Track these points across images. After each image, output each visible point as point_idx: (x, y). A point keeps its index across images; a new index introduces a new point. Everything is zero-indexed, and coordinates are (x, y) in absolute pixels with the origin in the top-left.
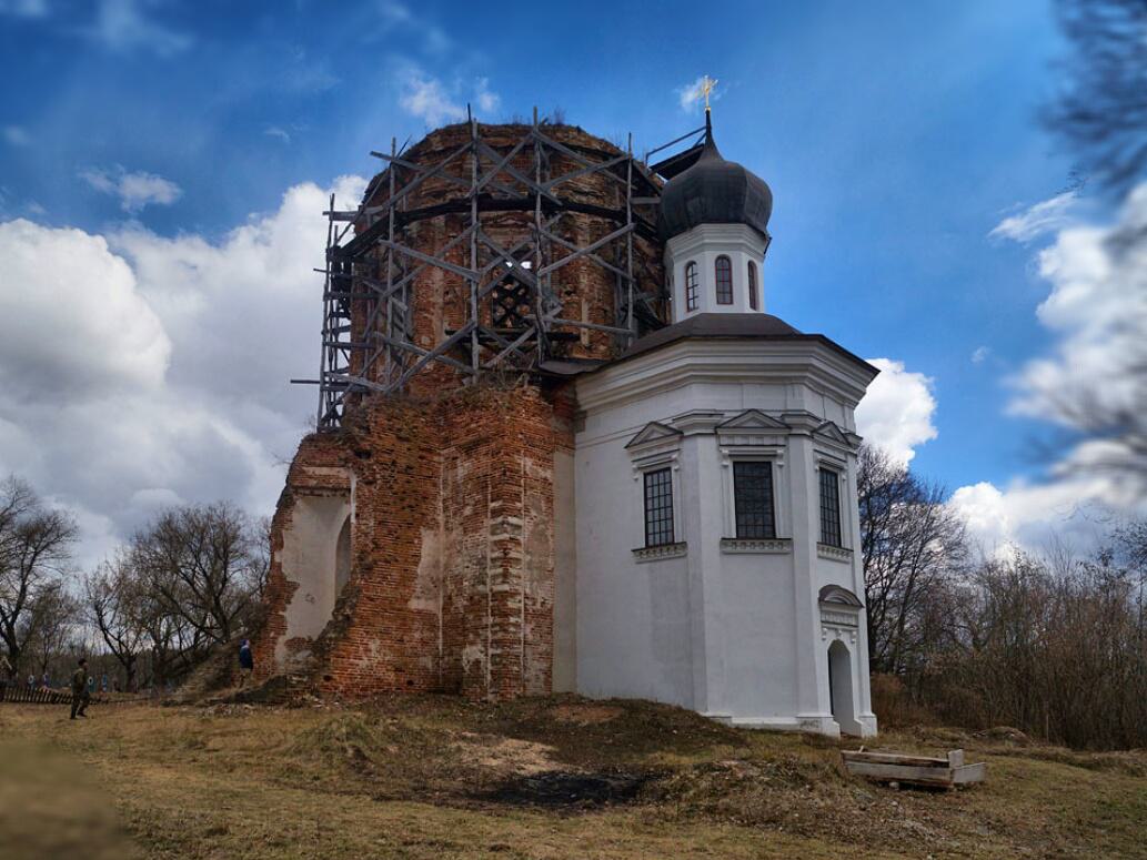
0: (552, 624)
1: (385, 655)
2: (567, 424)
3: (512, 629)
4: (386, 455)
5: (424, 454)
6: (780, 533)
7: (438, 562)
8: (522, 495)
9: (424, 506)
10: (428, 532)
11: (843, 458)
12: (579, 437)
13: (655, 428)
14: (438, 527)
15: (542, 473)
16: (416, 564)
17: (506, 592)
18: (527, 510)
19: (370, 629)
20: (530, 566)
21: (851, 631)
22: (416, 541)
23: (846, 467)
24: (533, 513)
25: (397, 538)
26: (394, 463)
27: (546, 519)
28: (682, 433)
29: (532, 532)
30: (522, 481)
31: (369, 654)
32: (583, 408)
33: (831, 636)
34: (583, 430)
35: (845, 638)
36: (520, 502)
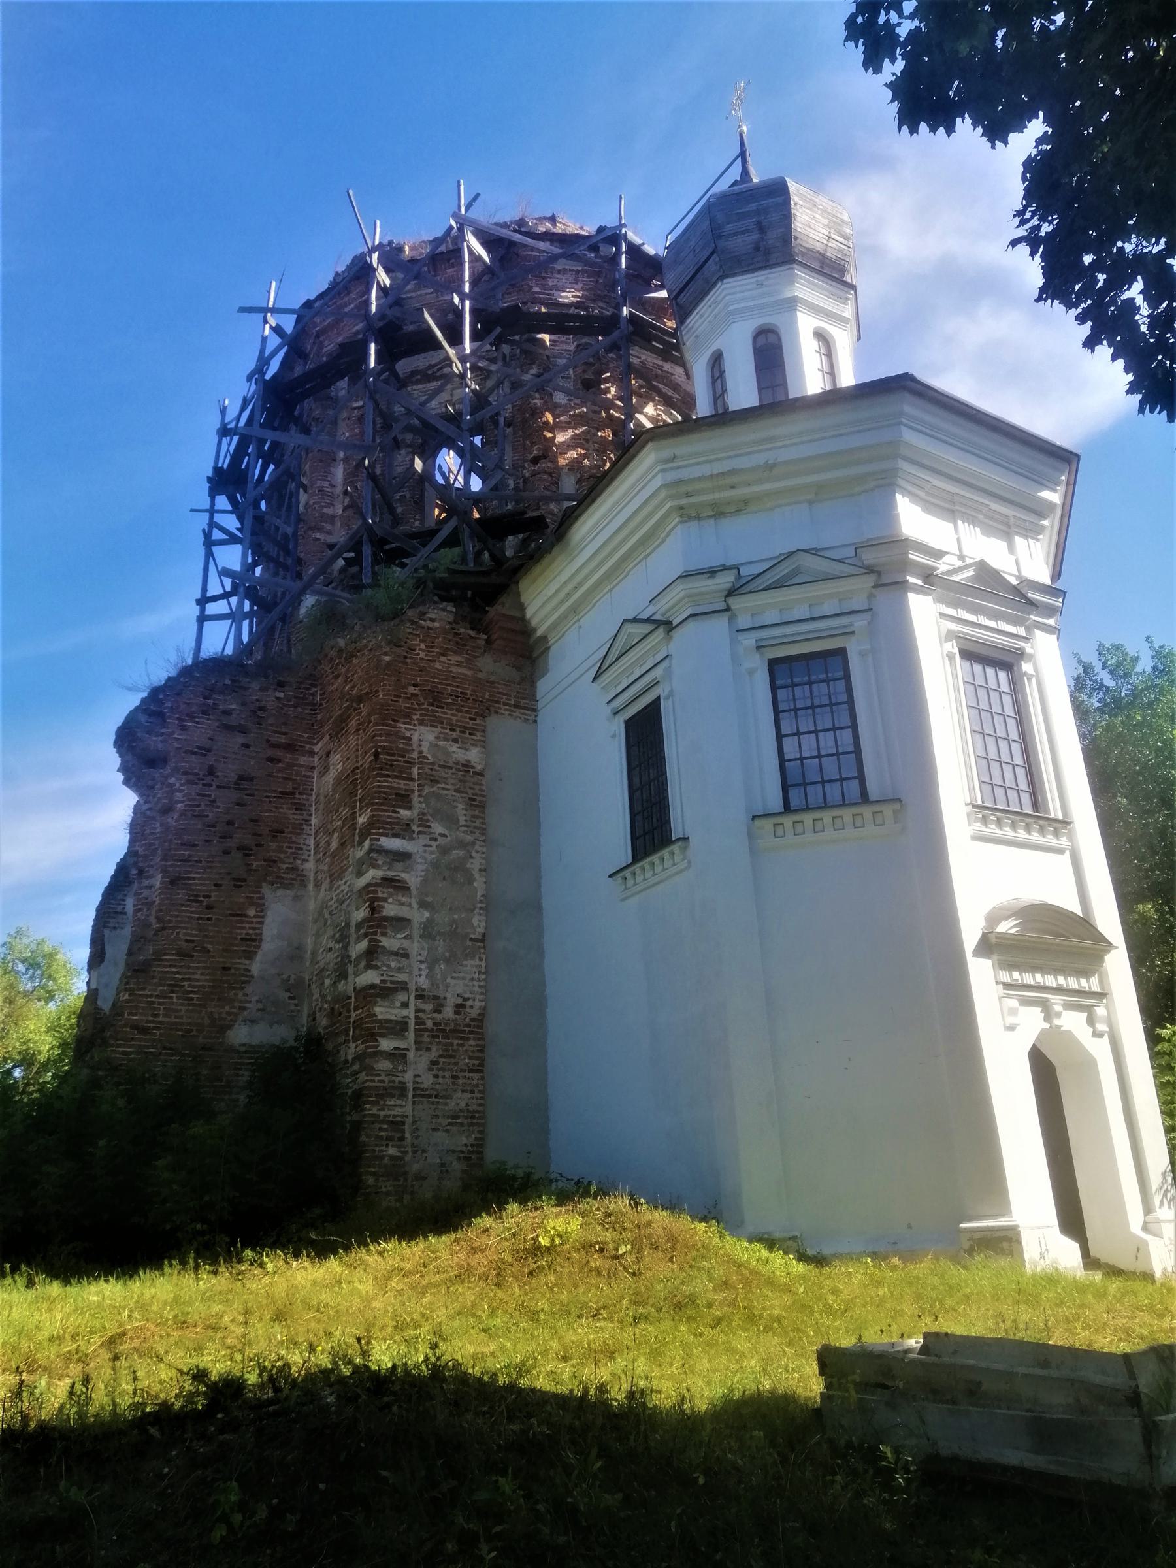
0: (482, 1049)
2: (519, 669)
3: (384, 1065)
4: (193, 758)
5: (278, 753)
7: (300, 948)
8: (415, 798)
9: (274, 845)
10: (280, 892)
11: (1022, 631)
12: (543, 686)
14: (304, 885)
15: (458, 753)
16: (250, 955)
17: (373, 986)
18: (424, 823)
20: (428, 931)
21: (1089, 1009)
22: (252, 912)
23: (1029, 650)
24: (437, 828)
25: (209, 907)
26: (211, 771)
27: (469, 838)
28: (671, 623)
29: (435, 865)
30: (415, 771)
32: (539, 633)
33: (1031, 1023)
34: (545, 672)
35: (1073, 1022)
36: (410, 808)
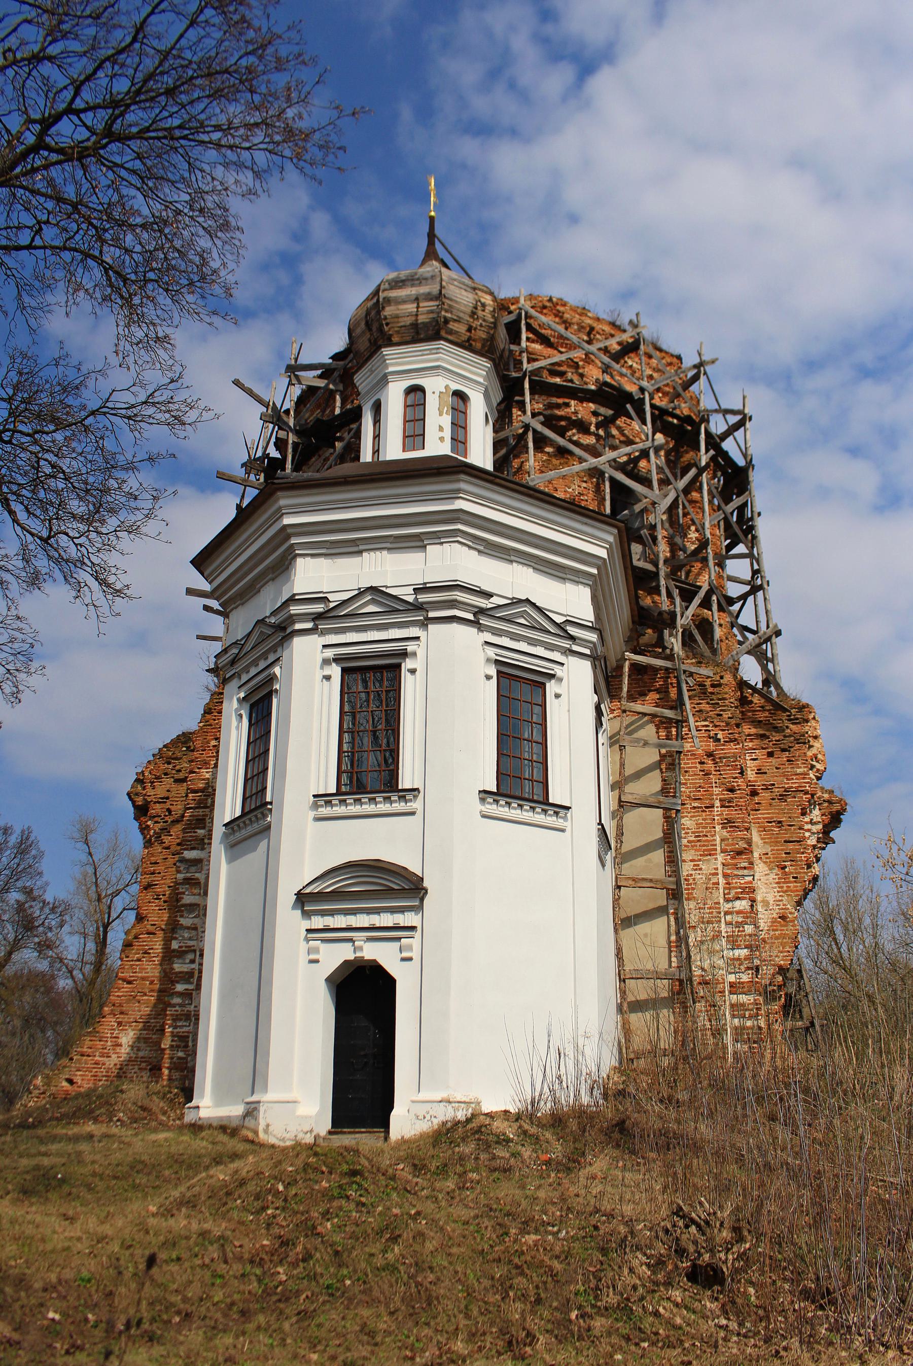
1: (139, 1050)
6: (406, 781)
13: (529, 609)
19: (121, 1018)
31: (118, 1049)
